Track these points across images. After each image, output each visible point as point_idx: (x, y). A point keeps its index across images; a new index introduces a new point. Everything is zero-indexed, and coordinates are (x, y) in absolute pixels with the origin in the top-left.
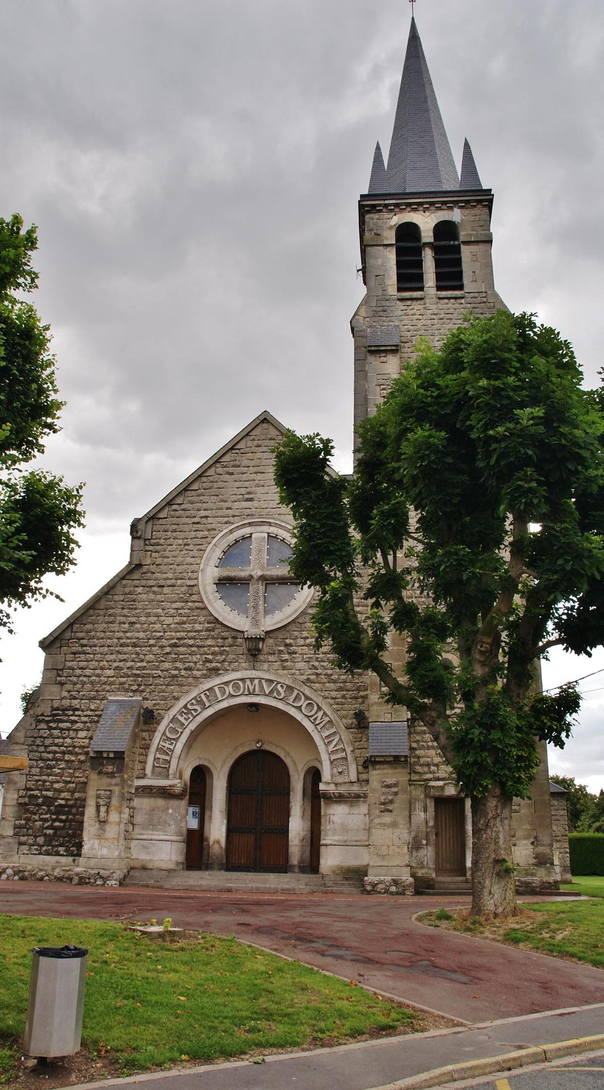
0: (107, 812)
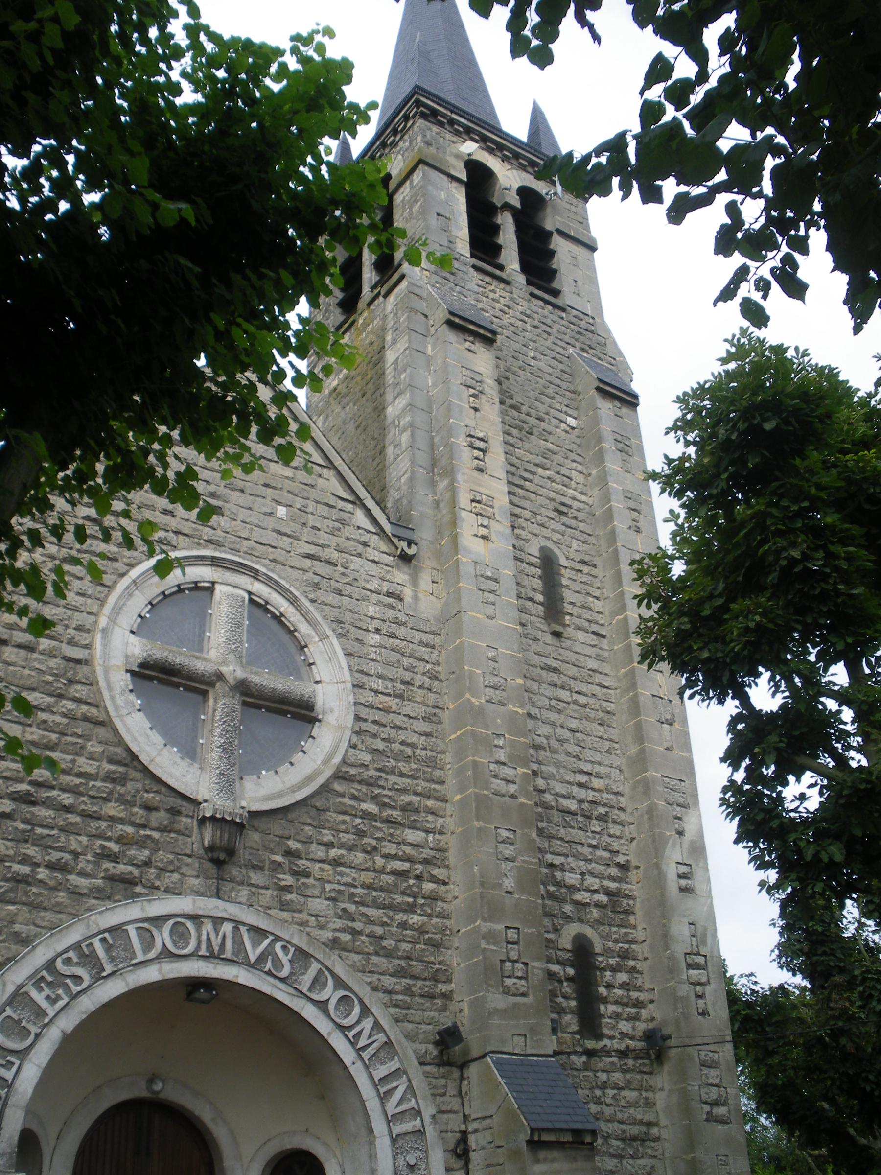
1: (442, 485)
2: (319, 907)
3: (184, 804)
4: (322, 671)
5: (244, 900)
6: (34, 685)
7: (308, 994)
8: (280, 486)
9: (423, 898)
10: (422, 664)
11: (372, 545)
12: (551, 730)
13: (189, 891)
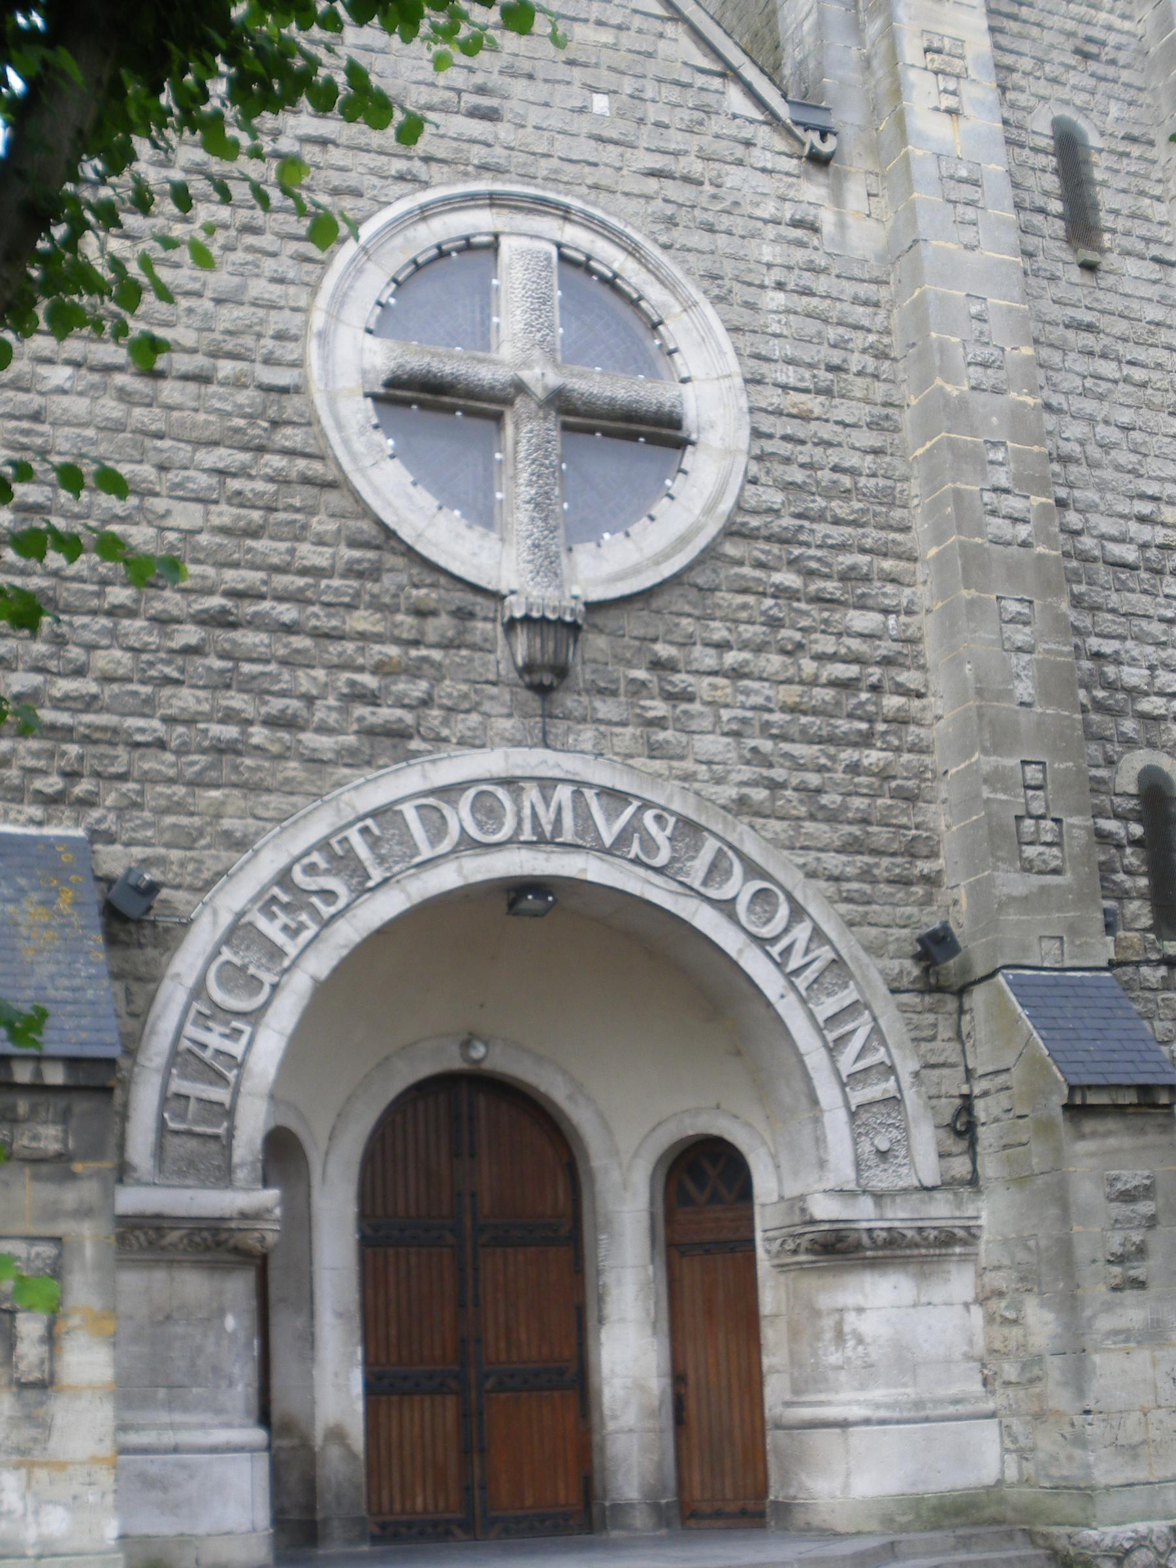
0: (51, 1339)
1: (873, 29)
2: (712, 748)
3: (479, 599)
4: (687, 363)
5: (588, 746)
6: (217, 437)
7: (702, 890)
8: (594, 60)
9: (885, 721)
10: (860, 334)
11: (760, 142)
12: (1086, 429)
13: (497, 740)
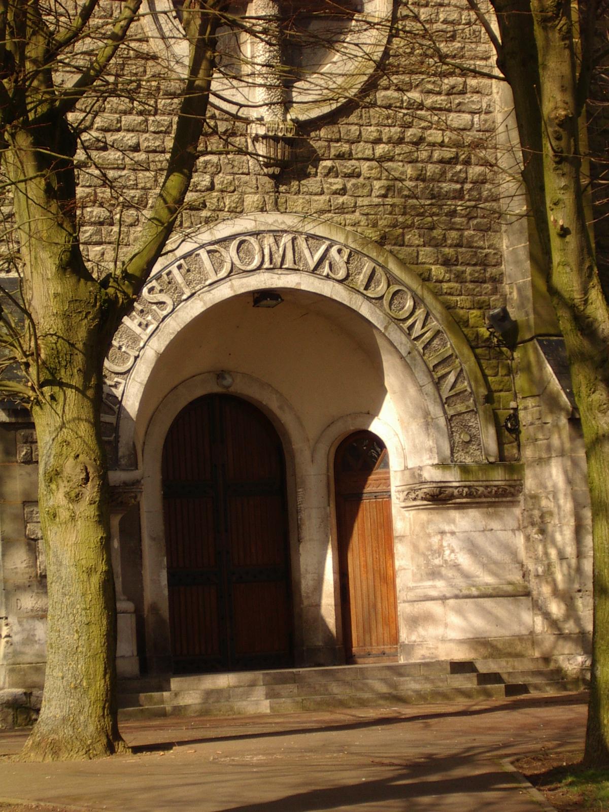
7: (365, 292)
